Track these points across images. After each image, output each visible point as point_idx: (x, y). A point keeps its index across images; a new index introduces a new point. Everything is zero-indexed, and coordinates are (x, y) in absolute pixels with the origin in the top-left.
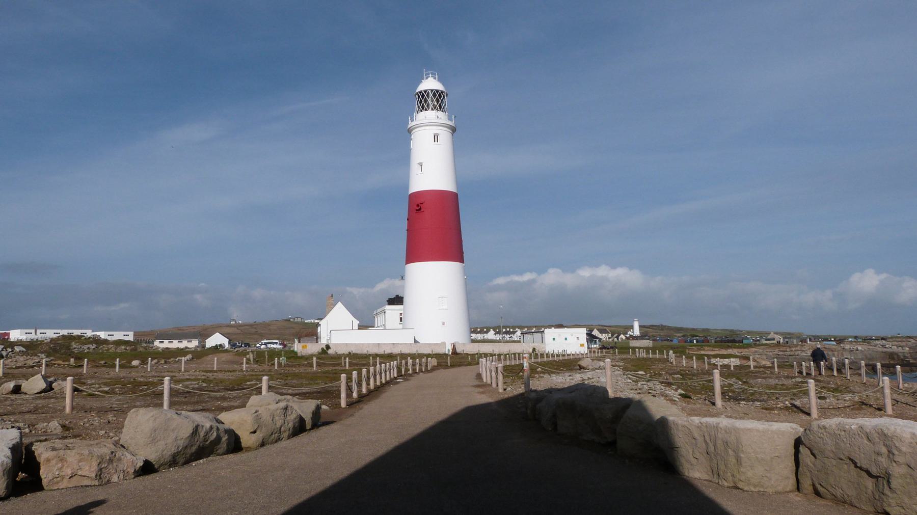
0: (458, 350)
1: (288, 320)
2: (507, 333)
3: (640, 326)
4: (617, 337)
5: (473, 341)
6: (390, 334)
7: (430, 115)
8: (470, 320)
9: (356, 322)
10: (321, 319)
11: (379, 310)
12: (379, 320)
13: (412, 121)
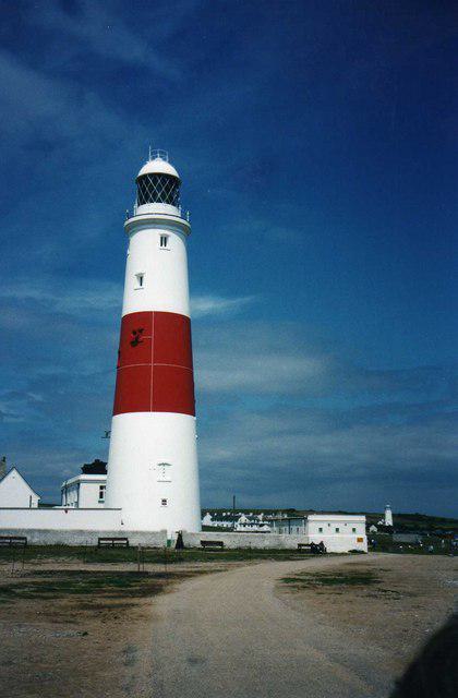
0: (186, 541)
3: (393, 515)
5: (205, 528)
8: (203, 502)
9: (36, 500)
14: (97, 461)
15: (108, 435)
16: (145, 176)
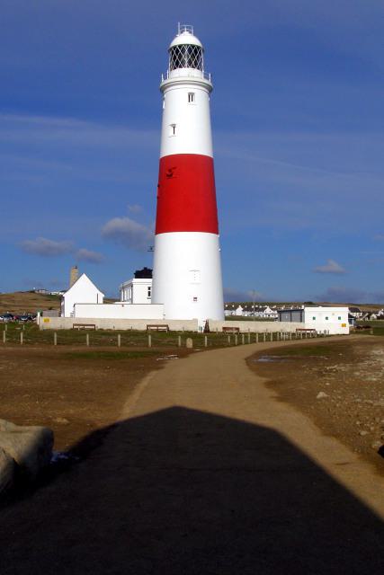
0: (211, 329)
1: (33, 292)
2: (257, 310)
4: (369, 317)
5: (227, 319)
6: (136, 310)
7: (185, 73)
9: (102, 296)
10: (65, 291)
11: (126, 283)
12: (126, 294)
13: (165, 78)
14: (145, 268)
16: (175, 47)
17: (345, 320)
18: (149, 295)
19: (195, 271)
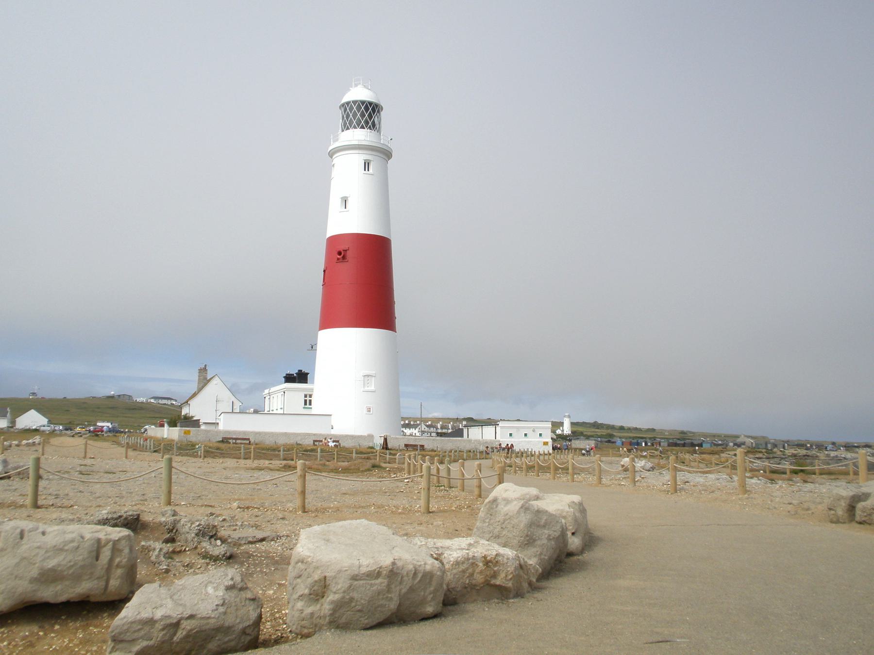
0: (390, 446)
3: (573, 424)
6: (281, 415)
11: (273, 389)
15: (313, 347)
16: (348, 103)
17: (548, 437)
18: (305, 404)
19: (368, 376)
